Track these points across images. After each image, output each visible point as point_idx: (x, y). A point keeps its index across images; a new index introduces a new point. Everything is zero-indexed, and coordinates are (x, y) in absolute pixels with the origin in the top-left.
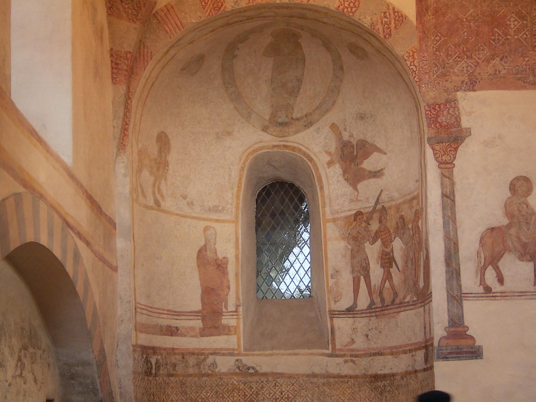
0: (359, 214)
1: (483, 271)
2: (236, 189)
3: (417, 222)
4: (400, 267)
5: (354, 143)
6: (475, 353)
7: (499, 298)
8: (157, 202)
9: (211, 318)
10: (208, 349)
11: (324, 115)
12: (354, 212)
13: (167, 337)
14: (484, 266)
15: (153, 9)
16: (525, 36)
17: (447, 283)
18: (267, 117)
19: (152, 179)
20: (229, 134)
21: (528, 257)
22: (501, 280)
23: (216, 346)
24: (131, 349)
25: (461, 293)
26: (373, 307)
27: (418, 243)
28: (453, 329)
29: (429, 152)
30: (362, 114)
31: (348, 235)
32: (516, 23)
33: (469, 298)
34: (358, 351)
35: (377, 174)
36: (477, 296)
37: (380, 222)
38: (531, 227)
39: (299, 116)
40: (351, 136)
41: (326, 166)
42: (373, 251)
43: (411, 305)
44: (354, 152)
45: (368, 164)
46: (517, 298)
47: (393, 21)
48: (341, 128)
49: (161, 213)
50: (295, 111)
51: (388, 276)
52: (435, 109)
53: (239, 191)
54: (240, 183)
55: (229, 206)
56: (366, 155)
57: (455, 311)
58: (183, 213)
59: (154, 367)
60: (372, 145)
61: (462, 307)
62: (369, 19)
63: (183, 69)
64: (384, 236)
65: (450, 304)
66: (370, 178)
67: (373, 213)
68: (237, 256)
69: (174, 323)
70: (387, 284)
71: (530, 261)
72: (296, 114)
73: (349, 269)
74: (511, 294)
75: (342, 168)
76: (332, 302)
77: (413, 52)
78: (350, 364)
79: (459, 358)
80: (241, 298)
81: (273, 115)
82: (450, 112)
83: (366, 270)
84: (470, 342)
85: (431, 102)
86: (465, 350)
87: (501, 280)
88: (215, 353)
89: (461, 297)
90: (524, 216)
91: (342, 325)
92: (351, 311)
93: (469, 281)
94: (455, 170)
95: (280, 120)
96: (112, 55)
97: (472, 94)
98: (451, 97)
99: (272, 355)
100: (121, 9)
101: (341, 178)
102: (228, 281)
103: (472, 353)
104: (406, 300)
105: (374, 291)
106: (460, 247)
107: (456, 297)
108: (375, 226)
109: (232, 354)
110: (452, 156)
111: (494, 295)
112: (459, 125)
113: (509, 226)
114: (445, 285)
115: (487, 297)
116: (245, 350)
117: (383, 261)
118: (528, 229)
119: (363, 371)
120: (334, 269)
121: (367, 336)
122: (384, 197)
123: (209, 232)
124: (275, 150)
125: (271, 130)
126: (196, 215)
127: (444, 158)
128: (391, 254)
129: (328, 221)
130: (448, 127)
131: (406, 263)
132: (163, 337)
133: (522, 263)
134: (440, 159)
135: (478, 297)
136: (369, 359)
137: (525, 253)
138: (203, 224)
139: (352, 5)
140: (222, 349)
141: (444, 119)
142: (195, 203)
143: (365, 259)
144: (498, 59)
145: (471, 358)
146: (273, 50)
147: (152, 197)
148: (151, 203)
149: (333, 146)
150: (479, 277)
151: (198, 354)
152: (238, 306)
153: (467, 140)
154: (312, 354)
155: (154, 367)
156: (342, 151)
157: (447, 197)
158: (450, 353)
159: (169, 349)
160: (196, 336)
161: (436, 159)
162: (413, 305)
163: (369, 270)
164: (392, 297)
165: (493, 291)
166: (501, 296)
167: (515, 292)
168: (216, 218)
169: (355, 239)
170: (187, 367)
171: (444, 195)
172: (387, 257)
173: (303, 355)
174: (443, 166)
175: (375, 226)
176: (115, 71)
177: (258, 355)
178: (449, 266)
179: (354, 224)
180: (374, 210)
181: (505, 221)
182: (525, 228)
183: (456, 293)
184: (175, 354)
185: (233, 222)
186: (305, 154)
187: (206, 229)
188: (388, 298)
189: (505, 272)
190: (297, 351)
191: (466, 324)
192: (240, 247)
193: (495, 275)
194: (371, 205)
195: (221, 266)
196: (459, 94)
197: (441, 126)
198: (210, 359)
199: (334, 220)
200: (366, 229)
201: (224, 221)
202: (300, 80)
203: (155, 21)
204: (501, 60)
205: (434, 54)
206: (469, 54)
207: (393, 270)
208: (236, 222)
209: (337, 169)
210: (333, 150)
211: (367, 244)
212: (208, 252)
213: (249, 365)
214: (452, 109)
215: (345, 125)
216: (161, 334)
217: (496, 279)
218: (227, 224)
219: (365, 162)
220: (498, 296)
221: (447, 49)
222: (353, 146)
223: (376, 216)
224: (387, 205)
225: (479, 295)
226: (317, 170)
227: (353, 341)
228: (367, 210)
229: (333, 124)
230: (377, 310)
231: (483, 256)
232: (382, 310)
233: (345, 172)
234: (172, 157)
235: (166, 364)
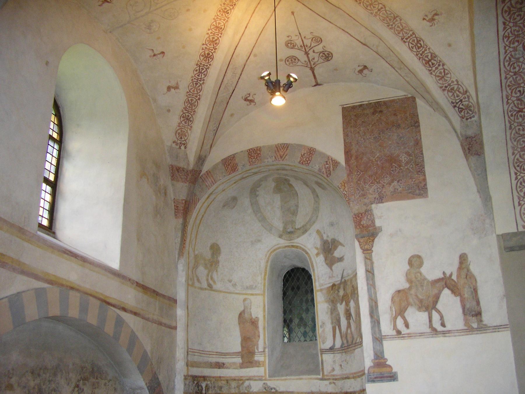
0: (334, 285)
2: (263, 274)
5: (330, 241)
6: (392, 377)
8: (210, 286)
9: (248, 356)
10: (245, 377)
12: (331, 284)
13: (216, 369)
15: (199, 174)
16: (411, 166)
18: (281, 229)
19: (206, 272)
20: (259, 241)
21: (424, 309)
22: (407, 326)
23: (251, 374)
24: (183, 377)
25: (382, 336)
28: (377, 361)
32: (406, 159)
34: (337, 376)
35: (341, 259)
36: (392, 338)
37: (344, 290)
38: (424, 288)
39: (299, 227)
40: (328, 237)
45: (337, 254)
47: (331, 167)
48: (322, 232)
49: (213, 292)
50: (297, 224)
51: (349, 326)
52: (359, 216)
53: (265, 275)
54: (266, 270)
55: (259, 285)
56: (336, 248)
57: (378, 348)
58: (229, 291)
59: (204, 389)
61: (382, 345)
62: (317, 166)
63: (224, 206)
66: (338, 262)
68: (264, 316)
69: (221, 360)
70: (349, 331)
71: (425, 311)
72: (297, 226)
73: (330, 321)
76: (321, 343)
77: (344, 183)
78: (333, 385)
79: (382, 381)
80: (267, 343)
81: (285, 228)
82: (369, 217)
83: (339, 321)
84: (388, 369)
85: (356, 212)
86: (386, 375)
87: (407, 326)
88: (250, 379)
89: (381, 339)
91: (327, 358)
92: (332, 349)
93: (386, 328)
94: (373, 254)
95: (289, 230)
96: (174, 202)
97: (381, 205)
98: (368, 208)
99: (286, 379)
100: (178, 176)
101: (324, 264)
102: (259, 332)
103: (390, 377)
106: (379, 305)
107: (378, 339)
108: (341, 293)
109: (261, 380)
112: (374, 226)
113: (410, 288)
114: (370, 330)
116: (270, 376)
119: (340, 390)
120: (322, 322)
121: (341, 366)
122: (345, 274)
123: (246, 302)
124: (286, 248)
125: (284, 237)
126: (238, 292)
127: (366, 247)
129: (318, 291)
130: (368, 227)
132: (213, 369)
133: (421, 313)
134: (363, 248)
136: (343, 381)
138: (242, 297)
139: (307, 159)
140: (254, 376)
141: (365, 222)
142: (237, 284)
144: (396, 182)
145: (390, 381)
146: (278, 189)
147: (206, 282)
148: (205, 285)
149: (319, 244)
151: (238, 380)
152: (265, 348)
153: (380, 234)
154: (311, 379)
155: (204, 389)
156: (324, 246)
157: (369, 272)
158: (376, 378)
159: (218, 377)
160: (237, 368)
161: (361, 248)
165: (403, 333)
167: (416, 333)
168: (251, 293)
169: (333, 302)
170: (230, 388)
171: (367, 271)
173: (306, 379)
175: (341, 293)
176: (176, 211)
177: (278, 380)
181: (407, 285)
182: (420, 289)
183: (378, 336)
184: (221, 380)
185: (262, 294)
186: (303, 250)
187: (245, 300)
188: (350, 340)
190: (301, 377)
191: (386, 356)
192: (266, 310)
195: (254, 323)
196: (373, 206)
197: (363, 227)
198: (247, 383)
199: (321, 290)
201: (256, 295)
202: (297, 206)
203: (201, 180)
204: (398, 182)
205: (357, 182)
206: (378, 180)
207: (351, 321)
208: (263, 295)
209: (321, 258)
210: (319, 246)
212: (246, 315)
213: (272, 386)
214: (369, 216)
216: (210, 368)
217: (404, 326)
218: (258, 297)
219: (335, 252)
221: (365, 179)
222: (329, 243)
223: (342, 286)
224: (346, 279)
226: (310, 259)
227: (333, 370)
231: (394, 310)
233: (326, 260)
234: (222, 258)
235: (215, 387)
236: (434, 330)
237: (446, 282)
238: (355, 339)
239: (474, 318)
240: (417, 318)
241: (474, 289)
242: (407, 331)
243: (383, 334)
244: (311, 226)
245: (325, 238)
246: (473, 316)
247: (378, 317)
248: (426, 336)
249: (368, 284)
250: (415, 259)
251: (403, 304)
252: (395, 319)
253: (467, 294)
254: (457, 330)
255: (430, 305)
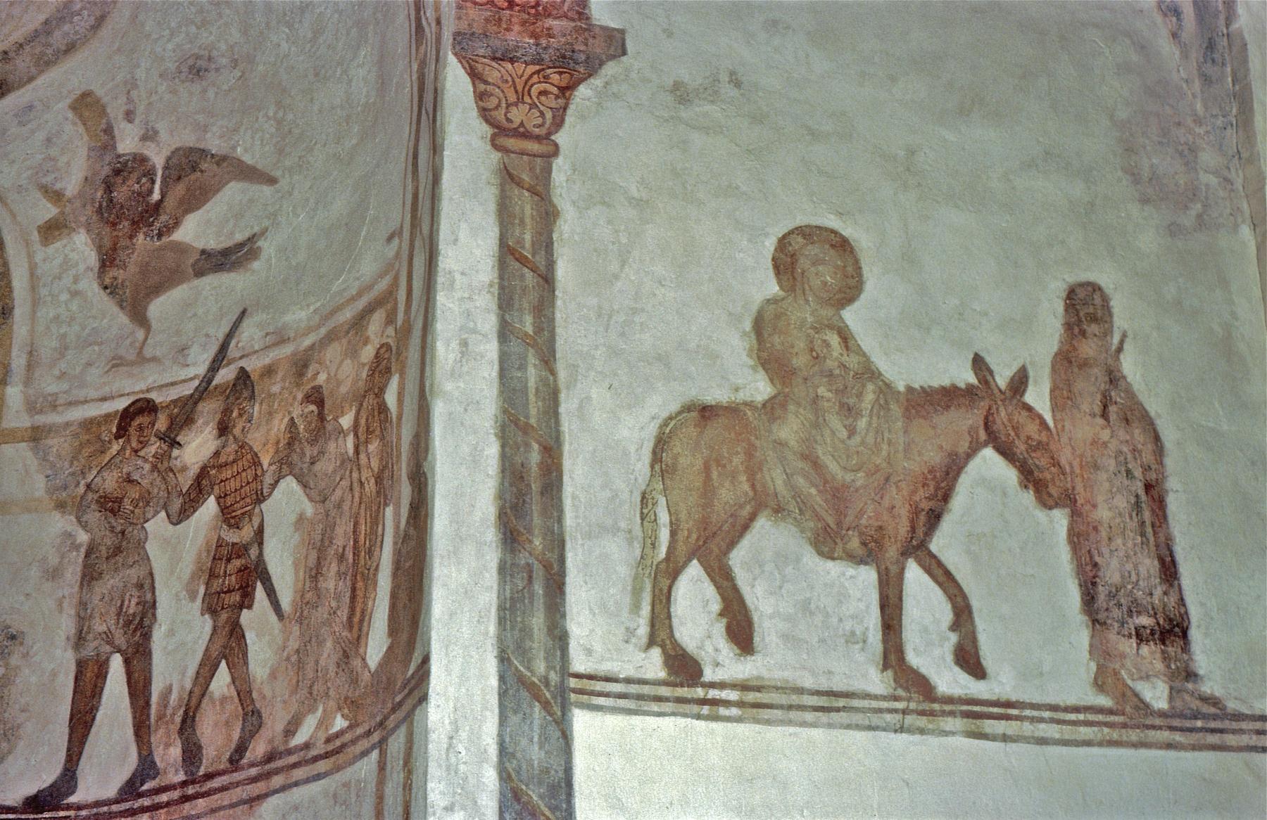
1: (664, 583)
3: (382, 390)
4: (286, 601)
7: (734, 711)
11: (55, 63)
12: (121, 404)
14: (667, 559)
17: (501, 621)
22: (742, 634)
25: (565, 672)
26: (145, 787)
27: (379, 479)
29: (456, 82)
30: (198, 57)
31: (82, 489)
33: (601, 701)
36: (635, 697)
37: (223, 429)
40: (149, 136)
41: (35, 236)
42: (176, 548)
43: (316, 759)
44: (151, 192)
46: (809, 716)
48: (115, 110)
57: (536, 754)
60: (224, 158)
61: (566, 738)
64: (233, 485)
65: (514, 719)
67: (196, 403)
70: (222, 680)
71: (861, 561)
74: (782, 699)
75: (99, 248)
83: (139, 627)
87: (742, 634)
89: (562, 691)
90: (831, 375)
93: (599, 630)
104: (299, 739)
105: (160, 717)
108: (198, 447)
110: (549, 115)
111: (713, 694)
113: (773, 409)
115: (680, 700)
117: (217, 584)
118: (852, 432)
128: (253, 552)
131: (316, 574)
135: (640, 697)
137: (839, 524)
143: (140, 586)
150: (646, 610)
156: (109, 188)
157: (522, 260)
161: (485, 114)
162: (327, 755)
163: (150, 627)
164: (236, 735)
165: (709, 675)
166: (740, 704)
167: (800, 691)
171: (508, 253)
172: (237, 563)
174: (511, 143)
178: (514, 540)
179: (115, 447)
180: (205, 389)
182: (835, 422)
183: (540, 667)
189: (760, 600)
193: (716, 606)
194: (191, 372)
200: (162, 466)
207: (257, 620)
211: (157, 525)
215: (130, 100)
217: (720, 628)
220: (727, 703)
222: (150, 174)
223: (209, 411)
224: (253, 365)
225: (646, 690)
228: (174, 394)
229: (86, 95)
230: (164, 798)
231: (664, 517)
232: (186, 799)
236: (915, 684)
237: (987, 407)
238: (275, 723)
239: (1145, 650)
240: (810, 598)
241: (1148, 487)
242: (743, 669)
243: (579, 664)
244: (44, 64)
245: (127, 143)
246: (1140, 636)
247: (558, 544)
248: (857, 718)
249: (505, 332)
250: (813, 250)
251: (729, 494)
252: (671, 570)
253: (1110, 505)
254: (1054, 708)
255: (897, 535)
